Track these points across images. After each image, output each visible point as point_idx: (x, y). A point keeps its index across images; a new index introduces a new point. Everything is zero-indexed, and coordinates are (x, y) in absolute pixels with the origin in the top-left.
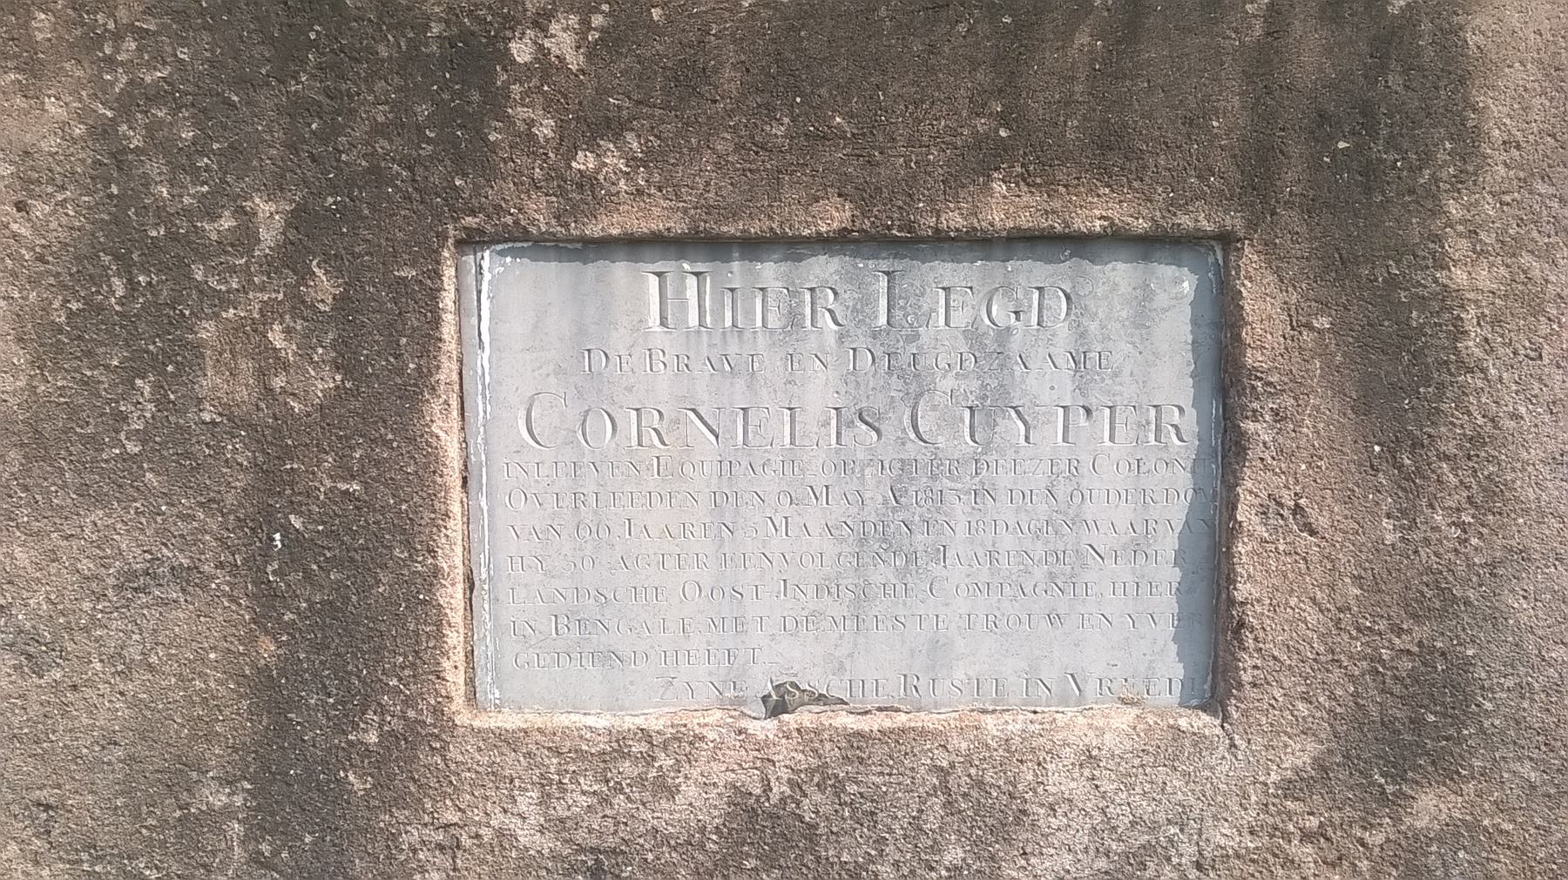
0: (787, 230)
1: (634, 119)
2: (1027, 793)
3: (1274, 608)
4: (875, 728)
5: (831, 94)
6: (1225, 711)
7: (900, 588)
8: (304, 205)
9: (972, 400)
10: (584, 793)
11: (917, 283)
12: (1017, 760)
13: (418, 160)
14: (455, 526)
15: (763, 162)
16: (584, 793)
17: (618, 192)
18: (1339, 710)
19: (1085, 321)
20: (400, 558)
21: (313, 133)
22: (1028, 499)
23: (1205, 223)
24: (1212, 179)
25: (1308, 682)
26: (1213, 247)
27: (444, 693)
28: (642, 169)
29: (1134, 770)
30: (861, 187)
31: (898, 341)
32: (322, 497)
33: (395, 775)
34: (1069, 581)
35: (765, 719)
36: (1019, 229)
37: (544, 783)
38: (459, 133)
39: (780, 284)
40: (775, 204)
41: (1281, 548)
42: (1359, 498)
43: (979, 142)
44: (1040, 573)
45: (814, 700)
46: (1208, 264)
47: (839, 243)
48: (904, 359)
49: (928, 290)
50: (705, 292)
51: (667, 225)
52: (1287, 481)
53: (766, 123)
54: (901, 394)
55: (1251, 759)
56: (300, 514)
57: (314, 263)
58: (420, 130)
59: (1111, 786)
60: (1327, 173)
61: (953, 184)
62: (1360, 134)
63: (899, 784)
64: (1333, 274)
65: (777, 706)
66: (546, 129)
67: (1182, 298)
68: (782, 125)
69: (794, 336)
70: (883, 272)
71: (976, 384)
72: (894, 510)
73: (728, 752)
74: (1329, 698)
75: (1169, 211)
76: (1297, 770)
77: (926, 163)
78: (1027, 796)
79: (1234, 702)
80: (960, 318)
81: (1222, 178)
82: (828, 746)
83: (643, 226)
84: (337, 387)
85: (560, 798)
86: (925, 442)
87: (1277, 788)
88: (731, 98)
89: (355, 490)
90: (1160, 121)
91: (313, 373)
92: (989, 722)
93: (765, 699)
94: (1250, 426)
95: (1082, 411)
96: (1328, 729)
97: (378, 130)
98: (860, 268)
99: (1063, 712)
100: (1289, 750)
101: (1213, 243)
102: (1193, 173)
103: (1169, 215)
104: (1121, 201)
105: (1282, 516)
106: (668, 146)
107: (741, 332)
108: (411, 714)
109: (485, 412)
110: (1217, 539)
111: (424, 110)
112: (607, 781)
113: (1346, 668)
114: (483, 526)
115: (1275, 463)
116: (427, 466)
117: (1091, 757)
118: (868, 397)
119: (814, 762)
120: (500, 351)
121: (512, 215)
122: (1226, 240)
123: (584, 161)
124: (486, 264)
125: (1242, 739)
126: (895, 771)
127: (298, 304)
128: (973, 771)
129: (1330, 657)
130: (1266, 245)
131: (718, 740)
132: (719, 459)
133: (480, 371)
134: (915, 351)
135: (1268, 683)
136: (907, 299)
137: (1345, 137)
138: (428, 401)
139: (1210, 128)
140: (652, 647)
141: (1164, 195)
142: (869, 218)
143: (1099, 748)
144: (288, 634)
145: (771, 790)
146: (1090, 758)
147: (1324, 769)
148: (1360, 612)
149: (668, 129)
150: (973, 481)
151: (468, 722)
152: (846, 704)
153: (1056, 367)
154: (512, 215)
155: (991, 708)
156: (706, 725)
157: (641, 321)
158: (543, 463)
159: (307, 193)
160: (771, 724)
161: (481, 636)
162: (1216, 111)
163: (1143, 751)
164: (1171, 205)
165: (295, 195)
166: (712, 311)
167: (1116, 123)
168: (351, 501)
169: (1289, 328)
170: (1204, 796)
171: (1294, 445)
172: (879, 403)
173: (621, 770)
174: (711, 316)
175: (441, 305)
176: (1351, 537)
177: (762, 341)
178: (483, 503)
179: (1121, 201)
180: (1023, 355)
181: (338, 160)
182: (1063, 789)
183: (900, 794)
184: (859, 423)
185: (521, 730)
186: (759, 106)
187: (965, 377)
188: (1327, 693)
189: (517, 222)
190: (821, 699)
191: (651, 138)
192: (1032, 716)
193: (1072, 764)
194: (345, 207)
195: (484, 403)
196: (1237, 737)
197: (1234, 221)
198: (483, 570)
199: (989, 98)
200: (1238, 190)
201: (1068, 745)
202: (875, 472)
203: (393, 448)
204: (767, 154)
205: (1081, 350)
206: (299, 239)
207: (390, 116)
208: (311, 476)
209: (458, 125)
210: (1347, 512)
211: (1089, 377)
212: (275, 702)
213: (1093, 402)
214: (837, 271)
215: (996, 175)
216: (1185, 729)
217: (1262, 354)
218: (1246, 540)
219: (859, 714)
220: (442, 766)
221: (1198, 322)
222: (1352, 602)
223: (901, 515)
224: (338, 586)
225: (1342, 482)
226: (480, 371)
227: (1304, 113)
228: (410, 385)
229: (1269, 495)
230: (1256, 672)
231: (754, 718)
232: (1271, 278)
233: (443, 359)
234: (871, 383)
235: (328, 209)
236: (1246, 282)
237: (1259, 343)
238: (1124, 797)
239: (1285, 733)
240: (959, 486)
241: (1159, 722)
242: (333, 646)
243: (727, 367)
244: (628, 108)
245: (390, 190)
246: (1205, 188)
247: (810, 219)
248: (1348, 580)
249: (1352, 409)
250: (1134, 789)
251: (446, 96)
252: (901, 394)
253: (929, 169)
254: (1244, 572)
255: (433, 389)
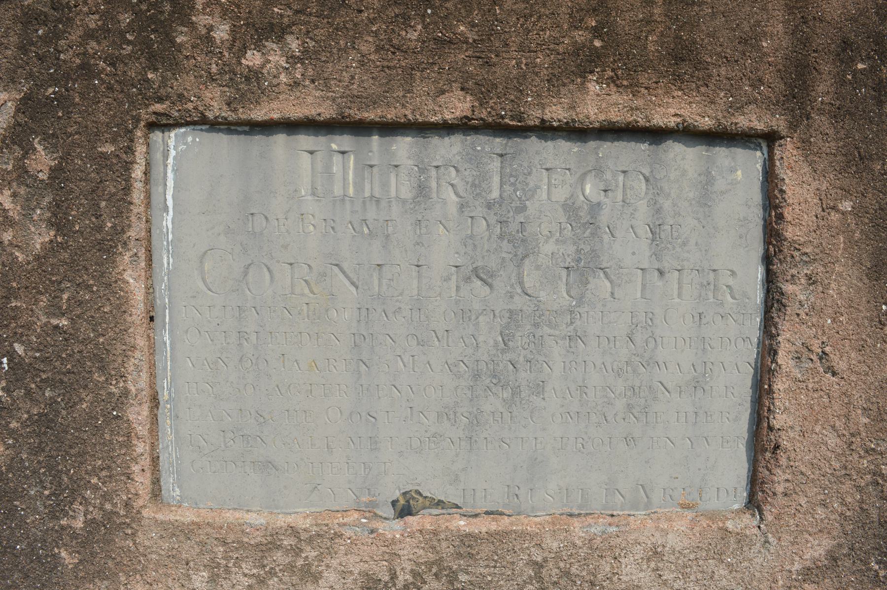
0: (418, 116)
1: (294, 25)
2: (605, 581)
3: (803, 433)
4: (484, 530)
5: (456, 7)
6: (761, 514)
7: (507, 415)
8: (30, 94)
9: (569, 262)
10: (245, 575)
11: (525, 164)
12: (598, 556)
13: (120, 59)
14: (138, 357)
15: (399, 60)
16: (245, 575)
17: (278, 84)
18: (848, 514)
19: (661, 200)
20: (98, 381)
21: (40, 37)
22: (612, 345)
23: (757, 123)
24: (762, 88)
25: (826, 491)
26: (760, 144)
27: (133, 491)
28: (299, 65)
29: (690, 562)
30: (480, 83)
31: (509, 212)
32: (38, 330)
33: (97, 553)
34: (643, 411)
35: (394, 519)
36: (610, 122)
37: (212, 565)
38: (152, 36)
39: (411, 162)
40: (408, 95)
41: (810, 386)
42: (870, 347)
43: (577, 50)
44: (620, 405)
45: (434, 505)
46: (756, 157)
47: (461, 129)
48: (513, 227)
49: (534, 170)
50: (349, 167)
51: (319, 111)
52: (817, 332)
53: (402, 29)
54: (511, 256)
55: (780, 552)
56: (22, 343)
57: (36, 140)
58: (122, 34)
59: (672, 576)
60: (849, 88)
61: (556, 82)
62: (874, 58)
63: (503, 574)
64: (854, 168)
65: (404, 511)
66: (222, 33)
67: (736, 184)
68: (415, 31)
69: (423, 206)
70: (497, 154)
71: (571, 249)
72: (503, 352)
73: (362, 547)
74: (842, 504)
75: (729, 113)
76: (814, 560)
77: (534, 65)
78: (604, 584)
79: (769, 507)
80: (561, 194)
81: (770, 87)
82: (444, 544)
83: (296, 112)
84: (51, 241)
85: (226, 578)
86: (530, 296)
87: (798, 574)
88: (374, 9)
89: (63, 325)
90: (721, 40)
91: (33, 229)
92: (576, 523)
93: (394, 503)
94: (788, 288)
95: (656, 273)
96: (839, 528)
97: (90, 35)
98: (478, 151)
99: (634, 515)
100: (809, 545)
101: (760, 141)
102: (747, 82)
103: (728, 115)
104: (691, 102)
105: (812, 360)
106: (321, 46)
107: (378, 201)
108: (108, 506)
109: (168, 264)
110: (759, 378)
111: (126, 18)
112: (264, 566)
113: (855, 480)
114: (166, 357)
115: (808, 318)
116: (119, 307)
117: (656, 553)
118: (483, 257)
119: (432, 557)
120: (181, 213)
121: (192, 102)
122: (771, 138)
123: (253, 58)
124: (172, 143)
125: (774, 536)
126: (498, 565)
127: (22, 173)
128: (562, 565)
129: (843, 472)
130: (803, 142)
131: (354, 537)
132: (358, 306)
133: (165, 230)
134: (523, 220)
135: (796, 493)
136: (516, 177)
137: (862, 60)
138: (121, 253)
139: (759, 48)
140: (302, 459)
141: (725, 99)
142: (486, 109)
143: (663, 545)
144: (14, 439)
145: (397, 578)
146: (656, 554)
147: (835, 559)
148: (868, 437)
149: (320, 33)
150: (569, 329)
151: (153, 515)
152: (457, 507)
153: (637, 237)
154: (192, 102)
155: (577, 512)
156: (345, 524)
157: (296, 191)
158: (214, 306)
159: (33, 85)
160: (398, 525)
161: (165, 445)
162: (765, 34)
163: (698, 547)
164: (730, 107)
165: (24, 86)
166: (355, 183)
167: (687, 39)
168: (61, 334)
169: (820, 209)
170: (743, 582)
171: (823, 304)
172: (493, 263)
173: (275, 558)
174: (354, 187)
175: (133, 176)
176: (862, 377)
177: (396, 209)
178: (167, 338)
179: (691, 102)
180: (611, 227)
181: (58, 59)
182: (634, 578)
183: (502, 582)
184: (475, 279)
185: (193, 523)
186: (397, 16)
187: (564, 242)
188: (840, 500)
189: (195, 108)
190: (439, 504)
191: (308, 40)
192: (609, 519)
193: (642, 558)
194: (62, 95)
195: (168, 257)
196: (770, 535)
197: (779, 123)
198: (166, 393)
199: (585, 15)
200: (782, 98)
201: (639, 544)
202: (489, 320)
203: (93, 292)
204: (403, 54)
205: (657, 223)
206: (25, 122)
207: (99, 23)
208: (30, 313)
209: (152, 30)
210: (860, 358)
211: (663, 245)
212: (4, 492)
213: (667, 264)
214: (459, 153)
215: (590, 77)
216: (731, 530)
217: (800, 230)
218: (784, 380)
219: (470, 516)
220: (133, 548)
221: (749, 203)
222: (862, 429)
223: (509, 356)
224: (53, 402)
225: (858, 333)
226: (165, 230)
227: (832, 39)
228: (108, 241)
229: (803, 344)
230: (787, 485)
231: (385, 518)
232: (806, 169)
233: (133, 219)
234: (486, 246)
235: (48, 98)
236: (788, 171)
237: (797, 221)
238: (681, 583)
239: (807, 531)
240: (557, 333)
241: (711, 523)
242: (48, 449)
243: (366, 230)
244: (289, 16)
245: (96, 82)
246: (757, 95)
247: (437, 108)
248: (859, 412)
249: (867, 276)
250: (689, 578)
251: (144, 7)
252: (511, 256)
253: (536, 70)
254: (781, 405)
255: (125, 243)
